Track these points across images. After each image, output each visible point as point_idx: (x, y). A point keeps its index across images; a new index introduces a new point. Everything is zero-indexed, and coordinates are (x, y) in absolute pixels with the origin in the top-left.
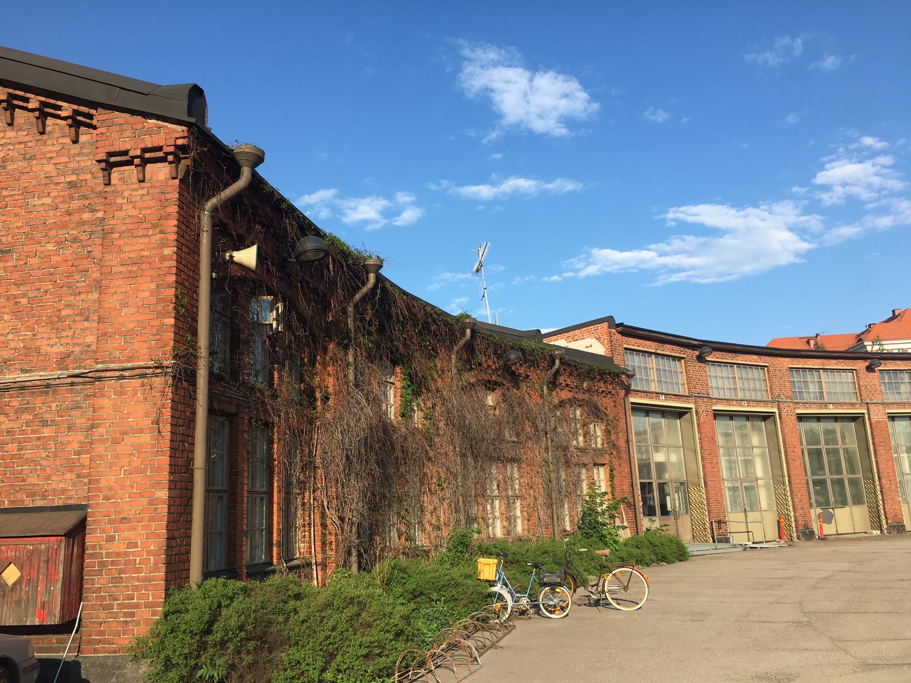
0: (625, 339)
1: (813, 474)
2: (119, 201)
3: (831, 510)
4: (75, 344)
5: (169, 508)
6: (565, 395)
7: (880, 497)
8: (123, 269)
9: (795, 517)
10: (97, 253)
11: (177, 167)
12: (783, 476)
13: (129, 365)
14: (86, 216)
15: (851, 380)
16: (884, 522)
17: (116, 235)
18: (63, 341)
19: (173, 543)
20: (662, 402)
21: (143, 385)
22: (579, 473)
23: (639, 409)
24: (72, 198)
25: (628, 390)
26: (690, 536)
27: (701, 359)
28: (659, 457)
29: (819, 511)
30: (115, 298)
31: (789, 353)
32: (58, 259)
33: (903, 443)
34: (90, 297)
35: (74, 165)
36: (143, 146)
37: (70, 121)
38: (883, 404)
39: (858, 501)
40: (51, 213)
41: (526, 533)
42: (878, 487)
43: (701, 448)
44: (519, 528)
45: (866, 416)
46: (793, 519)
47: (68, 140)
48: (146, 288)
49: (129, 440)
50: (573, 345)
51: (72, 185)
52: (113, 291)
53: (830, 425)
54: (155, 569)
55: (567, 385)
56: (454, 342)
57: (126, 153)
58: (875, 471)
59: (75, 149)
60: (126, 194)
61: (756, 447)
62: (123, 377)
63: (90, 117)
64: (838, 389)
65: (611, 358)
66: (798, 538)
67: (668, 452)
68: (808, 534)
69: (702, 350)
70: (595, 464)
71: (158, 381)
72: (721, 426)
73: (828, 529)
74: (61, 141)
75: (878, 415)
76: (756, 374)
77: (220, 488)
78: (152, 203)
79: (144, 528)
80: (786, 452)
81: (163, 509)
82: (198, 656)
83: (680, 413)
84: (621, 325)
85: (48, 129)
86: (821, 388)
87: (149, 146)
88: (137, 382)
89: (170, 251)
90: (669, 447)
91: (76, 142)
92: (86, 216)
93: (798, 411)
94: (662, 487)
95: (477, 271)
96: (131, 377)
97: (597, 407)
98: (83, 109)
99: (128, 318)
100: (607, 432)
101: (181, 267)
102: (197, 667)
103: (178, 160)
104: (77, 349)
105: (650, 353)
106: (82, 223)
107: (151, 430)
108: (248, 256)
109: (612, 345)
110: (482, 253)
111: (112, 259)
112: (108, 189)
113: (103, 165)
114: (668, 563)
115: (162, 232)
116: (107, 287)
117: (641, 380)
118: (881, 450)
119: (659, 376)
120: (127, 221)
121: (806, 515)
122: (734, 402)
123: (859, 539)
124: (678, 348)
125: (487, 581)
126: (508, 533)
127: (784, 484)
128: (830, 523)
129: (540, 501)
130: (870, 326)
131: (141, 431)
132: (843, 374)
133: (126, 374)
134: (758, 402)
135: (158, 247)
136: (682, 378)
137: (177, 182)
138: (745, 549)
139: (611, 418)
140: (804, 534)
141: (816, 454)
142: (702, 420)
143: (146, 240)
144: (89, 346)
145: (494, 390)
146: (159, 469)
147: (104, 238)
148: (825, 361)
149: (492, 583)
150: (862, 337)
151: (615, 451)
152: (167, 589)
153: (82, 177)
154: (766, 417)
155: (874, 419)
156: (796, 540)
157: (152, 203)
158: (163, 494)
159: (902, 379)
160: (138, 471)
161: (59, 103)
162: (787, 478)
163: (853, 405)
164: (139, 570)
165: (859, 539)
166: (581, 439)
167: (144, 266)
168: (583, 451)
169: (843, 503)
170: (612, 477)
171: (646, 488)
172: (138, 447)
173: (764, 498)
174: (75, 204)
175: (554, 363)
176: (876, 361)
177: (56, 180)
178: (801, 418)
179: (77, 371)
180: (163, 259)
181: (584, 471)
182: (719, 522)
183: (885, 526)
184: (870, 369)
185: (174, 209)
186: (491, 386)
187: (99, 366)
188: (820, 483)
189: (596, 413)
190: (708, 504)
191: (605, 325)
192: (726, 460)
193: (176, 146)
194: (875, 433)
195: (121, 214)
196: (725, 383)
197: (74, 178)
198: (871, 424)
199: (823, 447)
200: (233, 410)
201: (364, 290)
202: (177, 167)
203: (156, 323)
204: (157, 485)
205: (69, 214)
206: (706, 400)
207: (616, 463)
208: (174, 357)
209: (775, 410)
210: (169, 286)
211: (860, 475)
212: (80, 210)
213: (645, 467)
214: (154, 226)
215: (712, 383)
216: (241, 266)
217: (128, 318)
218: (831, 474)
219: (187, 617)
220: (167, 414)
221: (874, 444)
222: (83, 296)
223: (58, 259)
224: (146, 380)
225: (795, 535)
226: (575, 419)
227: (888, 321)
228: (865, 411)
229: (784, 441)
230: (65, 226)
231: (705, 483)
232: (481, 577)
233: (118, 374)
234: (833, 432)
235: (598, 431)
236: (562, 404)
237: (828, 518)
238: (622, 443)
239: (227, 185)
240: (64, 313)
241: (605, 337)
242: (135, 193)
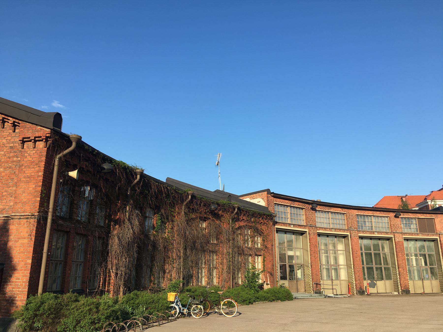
0: (275, 199)
1: (367, 264)
2: (26, 155)
3: (375, 282)
4: (7, 205)
5: (31, 266)
6: (242, 224)
7: (398, 277)
8: (24, 179)
9: (356, 284)
10: (17, 173)
11: (46, 144)
12: (351, 265)
13: (23, 214)
14: (15, 159)
15: (386, 221)
16: (400, 288)
17: (23, 167)
18: (3, 204)
19: (32, 279)
20: (292, 228)
21: (27, 222)
22: (248, 259)
23: (278, 231)
24: (11, 152)
25: (275, 223)
26: (304, 290)
27: (313, 209)
28: (291, 253)
29: (369, 282)
30: (21, 190)
31: (356, 208)
32: (4, 174)
33: (413, 252)
34: (13, 188)
35: (12, 140)
36: (35, 136)
37: (12, 125)
38: (402, 233)
39: (389, 277)
40: (3, 157)
41: (217, 284)
42: (398, 272)
43: (310, 250)
44: (215, 281)
45: (393, 239)
46: (355, 285)
47: (11, 131)
48: (32, 186)
49: (20, 241)
50: (253, 201)
51: (11, 147)
52: (20, 187)
53: (375, 242)
54: (25, 288)
55: (243, 219)
56: (182, 202)
57: (29, 138)
58: (397, 264)
59: (14, 134)
60: (28, 152)
61: (331, 250)
62: (20, 218)
63: (19, 124)
64: (380, 225)
65: (268, 208)
66: (357, 294)
67: (298, 252)
68: (361, 292)
69: (314, 205)
70: (256, 255)
71: (32, 220)
72: (322, 240)
73: (372, 290)
74: (9, 131)
75: (399, 238)
76: (340, 216)
77: (61, 259)
78: (37, 156)
79: (22, 273)
80: (353, 253)
81: (29, 267)
82: (34, 319)
83: (302, 233)
84: (273, 193)
85: (5, 126)
86: (372, 225)
87: (37, 136)
88: (25, 220)
89: (41, 174)
90: (295, 248)
91: (14, 131)
92: (15, 159)
93: (359, 235)
94: (291, 267)
95: (218, 165)
96: (23, 219)
97: (257, 229)
98: (17, 121)
99: (24, 197)
100: (264, 240)
101: (45, 179)
102: (34, 323)
103: (47, 141)
104: (7, 207)
105: (288, 206)
106: (14, 161)
107: (28, 238)
108: (74, 174)
109: (268, 202)
110: (219, 158)
111: (21, 176)
112: (23, 150)
113: (21, 142)
114: (282, 301)
115: (39, 167)
116: (19, 186)
117: (282, 218)
118: (400, 255)
119: (291, 216)
120: (28, 162)
121: (361, 283)
122: (328, 229)
123: (388, 296)
124: (302, 204)
125: (171, 302)
126: (208, 284)
127: (351, 268)
128: (374, 287)
129: (225, 270)
130: (432, 192)
131: (25, 238)
132: (383, 218)
133: (22, 217)
134: (340, 230)
135: (37, 172)
136: (304, 217)
137: (46, 149)
138: (325, 297)
139: (265, 234)
140: (359, 292)
141: (369, 255)
142: (311, 237)
143: (33, 169)
144: (11, 206)
145: (206, 221)
146: (29, 252)
147: (19, 168)
148: (374, 212)
149: (173, 303)
150: (427, 198)
151: (266, 251)
152: (28, 295)
153: (15, 145)
154: (345, 237)
155: (397, 240)
156: (355, 294)
157: (37, 156)
158: (30, 261)
159: (412, 222)
160: (22, 252)
161: (9, 118)
162: (352, 266)
163: (387, 233)
164: (19, 288)
165: (388, 296)
166: (250, 243)
167: (32, 179)
168: (250, 249)
169: (382, 279)
170: (264, 261)
171: (283, 267)
172: (23, 244)
173: (343, 274)
174: (12, 155)
175: (235, 209)
176: (398, 213)
177: (6, 145)
178: (362, 238)
179: (6, 215)
180: (39, 176)
181: (250, 258)
182: (317, 284)
183: (400, 291)
184: (396, 216)
185: (44, 159)
186: (204, 219)
187: (13, 214)
188: (370, 269)
189: (260, 233)
190: (312, 275)
191: (266, 193)
192: (325, 256)
193: (46, 137)
194: (397, 247)
195: (25, 159)
196: (323, 220)
197: (12, 145)
198: (395, 242)
199: (373, 252)
200: (68, 230)
201: (136, 181)
202: (46, 144)
203: (34, 199)
204: (28, 258)
205: (9, 158)
206: (314, 228)
207: (267, 255)
208: (38, 212)
209: (348, 234)
210: (39, 186)
211: (390, 266)
212: (13, 157)
213: (282, 257)
214: (37, 164)
215: (318, 220)
216: (71, 177)
217: (24, 197)
218: (376, 264)
219: (32, 304)
220: (34, 234)
221: (396, 252)
222: (11, 188)
223: (4, 174)
224: (28, 220)
225: (355, 292)
226: (247, 234)
227: (440, 190)
228: (393, 236)
229: (352, 248)
230: (7, 162)
231: (311, 266)
232: (168, 300)
233: (19, 217)
234: (378, 245)
235: (259, 240)
236: (240, 228)
237: (373, 285)
238: (269, 246)
239: (66, 149)
240: (4, 194)
241: (266, 198)
242: (32, 152)
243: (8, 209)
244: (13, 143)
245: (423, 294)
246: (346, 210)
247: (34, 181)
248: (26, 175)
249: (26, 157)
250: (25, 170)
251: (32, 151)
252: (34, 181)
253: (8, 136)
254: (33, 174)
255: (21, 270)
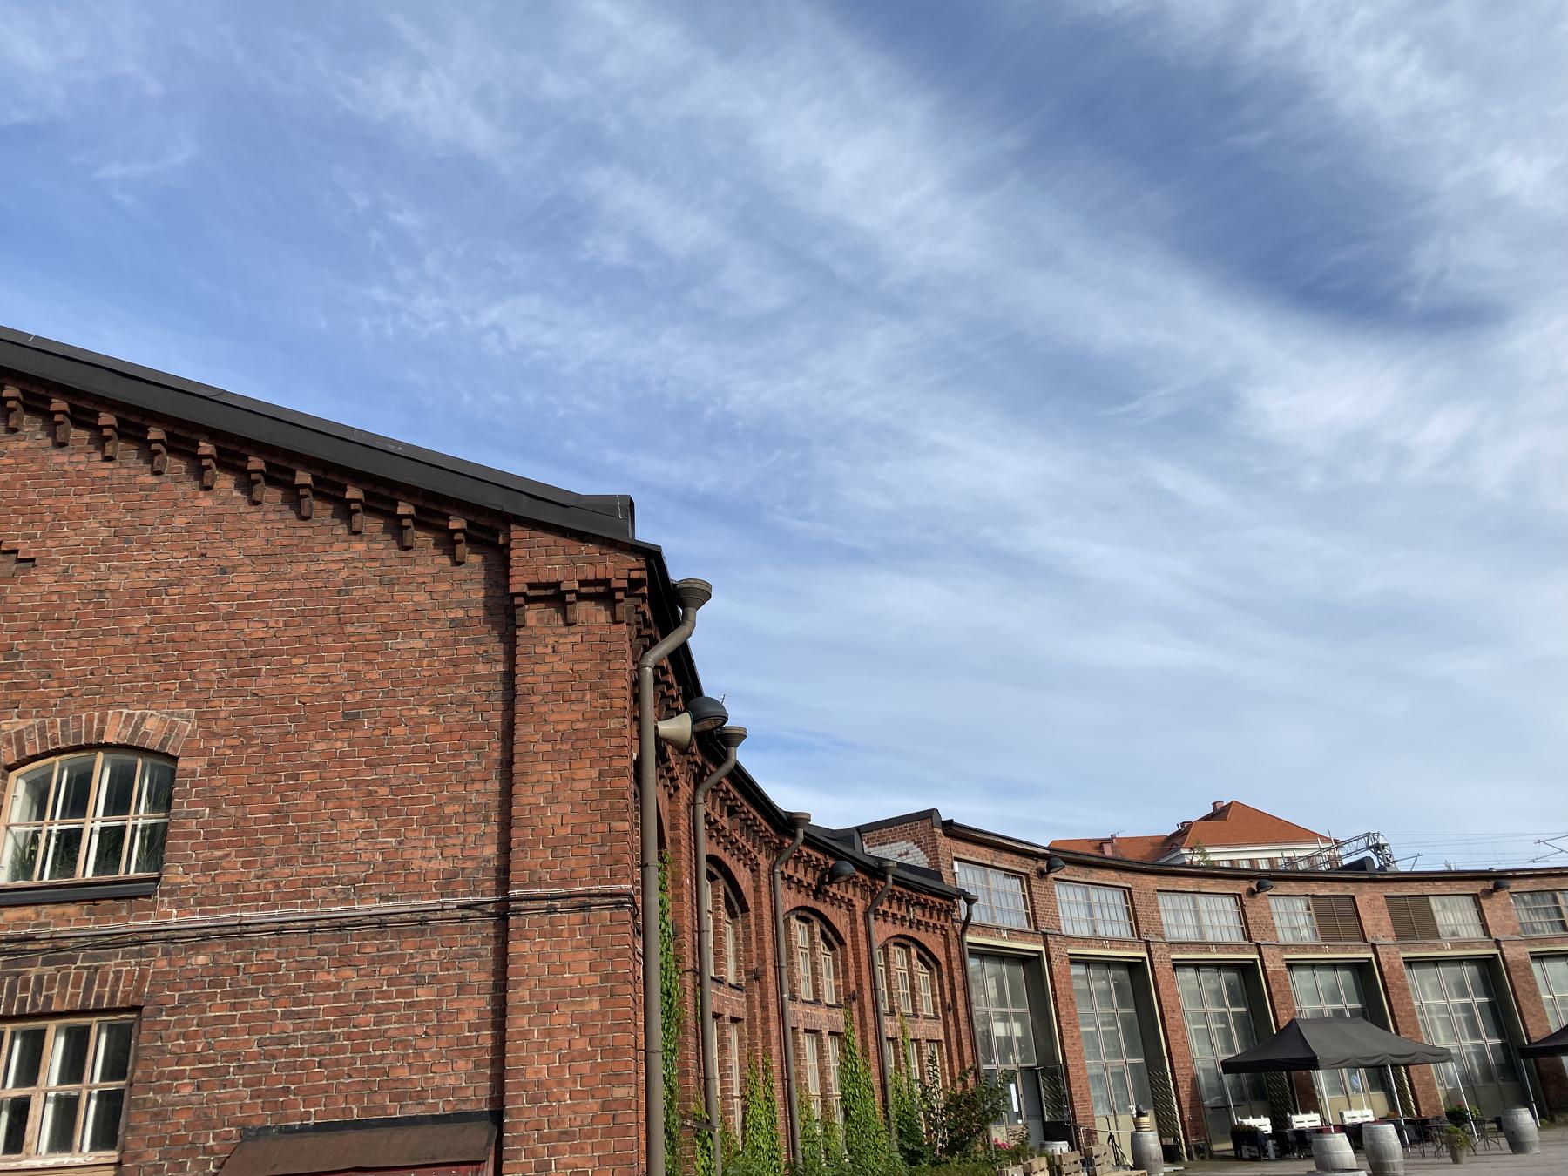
0: (954, 843)
2: (539, 650)
24: (457, 642)
32: (439, 728)
36: (581, 577)
52: (535, 779)
78: (587, 655)
92: (480, 668)
104: (469, 865)
106: (478, 678)
124: (1014, 857)
133: (558, 904)
148: (1200, 881)
155: (1270, 967)
160: (583, 1055)
193: (630, 581)
197: (460, 613)
203: (600, 827)
212: (471, 660)
222: (478, 786)
230: (447, 681)
233: (545, 904)
240: (449, 810)
243: (476, 870)
244: (460, 605)
245: (304, 1129)
246: (1129, 876)
247: (594, 754)
248: (549, 728)
249: (542, 660)
250: (544, 709)
251: (565, 636)
252: (594, 754)
253: (436, 578)
254: (580, 726)
255: (591, 1135)
